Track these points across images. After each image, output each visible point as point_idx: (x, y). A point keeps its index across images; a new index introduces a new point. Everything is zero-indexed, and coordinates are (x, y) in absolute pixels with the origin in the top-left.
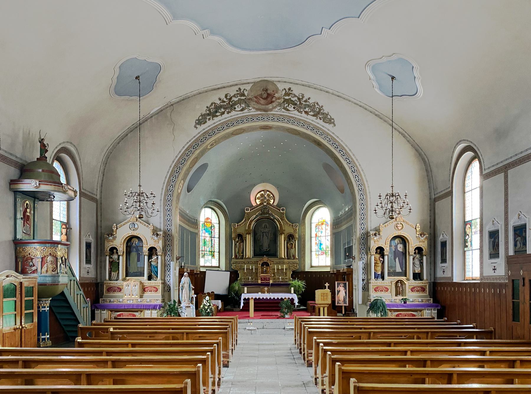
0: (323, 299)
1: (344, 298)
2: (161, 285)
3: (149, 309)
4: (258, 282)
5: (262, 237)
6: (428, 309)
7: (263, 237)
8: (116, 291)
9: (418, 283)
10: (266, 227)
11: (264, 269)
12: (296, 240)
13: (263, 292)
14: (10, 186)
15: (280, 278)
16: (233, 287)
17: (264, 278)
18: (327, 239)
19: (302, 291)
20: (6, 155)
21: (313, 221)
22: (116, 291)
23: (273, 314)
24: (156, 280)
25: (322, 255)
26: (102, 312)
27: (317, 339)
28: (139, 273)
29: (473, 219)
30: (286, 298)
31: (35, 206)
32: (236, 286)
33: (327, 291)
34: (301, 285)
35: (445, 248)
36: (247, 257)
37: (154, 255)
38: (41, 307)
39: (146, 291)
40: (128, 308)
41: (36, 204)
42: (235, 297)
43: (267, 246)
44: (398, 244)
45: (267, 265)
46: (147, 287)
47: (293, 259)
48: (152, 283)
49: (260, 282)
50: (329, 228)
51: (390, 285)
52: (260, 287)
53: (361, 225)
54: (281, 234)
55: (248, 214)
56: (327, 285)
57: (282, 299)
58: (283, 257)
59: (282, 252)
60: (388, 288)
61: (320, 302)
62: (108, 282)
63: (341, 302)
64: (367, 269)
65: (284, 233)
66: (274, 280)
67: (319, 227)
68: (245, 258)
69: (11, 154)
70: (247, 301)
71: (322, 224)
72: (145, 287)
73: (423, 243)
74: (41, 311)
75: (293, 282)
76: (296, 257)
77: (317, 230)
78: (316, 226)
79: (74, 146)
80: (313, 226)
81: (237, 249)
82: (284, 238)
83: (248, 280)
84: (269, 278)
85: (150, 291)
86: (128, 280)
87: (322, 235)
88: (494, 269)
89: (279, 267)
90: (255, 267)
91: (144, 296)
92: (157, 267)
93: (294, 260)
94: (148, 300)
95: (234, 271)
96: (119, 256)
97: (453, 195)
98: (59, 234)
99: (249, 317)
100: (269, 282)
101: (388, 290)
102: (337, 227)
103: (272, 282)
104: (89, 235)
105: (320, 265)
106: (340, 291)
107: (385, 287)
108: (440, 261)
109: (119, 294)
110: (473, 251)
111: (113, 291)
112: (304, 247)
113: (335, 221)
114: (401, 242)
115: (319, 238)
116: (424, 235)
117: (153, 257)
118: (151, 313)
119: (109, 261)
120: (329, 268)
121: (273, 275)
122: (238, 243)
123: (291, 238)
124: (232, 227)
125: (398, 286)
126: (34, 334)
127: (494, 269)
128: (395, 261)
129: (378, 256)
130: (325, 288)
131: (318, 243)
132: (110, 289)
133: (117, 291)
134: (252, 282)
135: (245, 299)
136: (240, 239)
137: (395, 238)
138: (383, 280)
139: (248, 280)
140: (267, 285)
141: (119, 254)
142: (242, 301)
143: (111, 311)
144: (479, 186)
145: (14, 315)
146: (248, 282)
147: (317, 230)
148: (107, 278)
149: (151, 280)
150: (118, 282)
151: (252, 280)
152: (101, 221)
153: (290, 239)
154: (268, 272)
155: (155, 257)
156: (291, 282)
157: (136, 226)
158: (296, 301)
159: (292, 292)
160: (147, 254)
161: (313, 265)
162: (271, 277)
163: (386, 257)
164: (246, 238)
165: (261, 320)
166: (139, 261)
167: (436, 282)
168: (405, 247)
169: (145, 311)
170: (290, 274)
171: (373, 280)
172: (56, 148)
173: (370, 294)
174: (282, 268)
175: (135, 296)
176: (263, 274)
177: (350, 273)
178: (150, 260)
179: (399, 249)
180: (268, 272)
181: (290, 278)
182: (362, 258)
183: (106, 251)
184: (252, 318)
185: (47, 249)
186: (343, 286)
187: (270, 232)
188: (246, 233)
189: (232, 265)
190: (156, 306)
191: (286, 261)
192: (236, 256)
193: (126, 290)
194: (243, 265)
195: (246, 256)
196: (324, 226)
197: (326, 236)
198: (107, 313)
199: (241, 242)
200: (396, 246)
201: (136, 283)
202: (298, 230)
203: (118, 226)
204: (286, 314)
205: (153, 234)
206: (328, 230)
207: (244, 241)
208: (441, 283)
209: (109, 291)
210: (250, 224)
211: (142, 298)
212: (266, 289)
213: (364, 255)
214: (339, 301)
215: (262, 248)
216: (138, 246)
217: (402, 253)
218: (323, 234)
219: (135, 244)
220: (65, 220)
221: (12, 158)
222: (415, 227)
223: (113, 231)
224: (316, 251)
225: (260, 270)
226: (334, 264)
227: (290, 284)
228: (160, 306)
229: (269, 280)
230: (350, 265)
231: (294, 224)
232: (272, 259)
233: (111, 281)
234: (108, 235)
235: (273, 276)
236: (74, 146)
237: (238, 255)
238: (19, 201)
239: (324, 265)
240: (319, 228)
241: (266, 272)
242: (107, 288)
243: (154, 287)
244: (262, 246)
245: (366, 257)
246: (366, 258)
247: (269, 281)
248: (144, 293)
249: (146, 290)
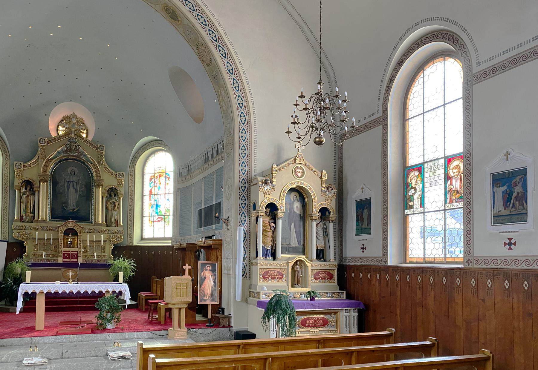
0: (179, 294)
1: (212, 290)
4: (58, 260)
5: (66, 188)
6: (345, 310)
7: (68, 190)
9: (320, 265)
10: (73, 173)
11: (69, 240)
12: (120, 198)
13: (66, 280)
15: (95, 254)
16: (12, 270)
17: (68, 254)
18: (167, 198)
19: (130, 277)
21: (146, 171)
23: (84, 319)
25: (159, 221)
27: (157, 358)
29: (426, 160)
30: (108, 292)
32: (17, 267)
33: (187, 278)
34: (129, 267)
35: (365, 211)
36: (40, 219)
42: (12, 286)
43: (75, 204)
44: (294, 201)
45: (75, 233)
47: (116, 226)
49: (60, 260)
50: (171, 183)
51: (286, 268)
52: (61, 269)
53: (242, 166)
54: (98, 186)
55: (43, 149)
56: (187, 267)
57: (101, 293)
58: (100, 222)
59: (99, 216)
60: (283, 273)
61: (175, 300)
63: (207, 299)
64: (248, 240)
65: (102, 185)
66: (84, 259)
67: (156, 180)
68: (37, 221)
70: (30, 298)
71: (160, 176)
73: (330, 202)
75: (116, 262)
76: (120, 223)
77: (152, 185)
78: (151, 179)
80: (147, 178)
81: (23, 207)
82: (102, 193)
83: (40, 258)
84: (77, 255)
87: (160, 192)
89: (93, 237)
90: (53, 236)
93: (116, 228)
95: (17, 241)
97: (387, 125)
99: (32, 329)
100: (77, 262)
101: (283, 277)
102: (187, 178)
103: (81, 262)
105: (156, 236)
106: (205, 278)
107: (278, 272)
108: (354, 232)
110: (426, 214)
112: (133, 210)
113: (181, 171)
114: (298, 199)
115: (156, 196)
116: (332, 190)
120: (171, 242)
121: (83, 250)
122: (25, 196)
123: (112, 194)
124: (15, 168)
125: (296, 269)
128: (290, 229)
129: (268, 219)
130: (184, 274)
131: (153, 204)
134: (48, 260)
135: (26, 294)
136: (28, 189)
137: (292, 190)
138: (274, 259)
139: (40, 258)
140: (74, 266)
142: (20, 299)
144: (462, 96)
146: (41, 260)
147: (152, 185)
151: (48, 258)
153: (110, 196)
154: (76, 244)
156: (112, 262)
158: (127, 296)
159: (121, 279)
161: (146, 235)
162: (80, 252)
163: (280, 222)
164: (39, 187)
165: (58, 337)
167: (346, 265)
168: (304, 206)
170: (109, 248)
171: (260, 258)
173: (253, 283)
174: (99, 239)
176: (68, 247)
177: (217, 246)
179: (295, 210)
180: (76, 244)
181: (110, 256)
182: (242, 221)
184: (41, 334)
186: (210, 270)
187: (80, 182)
188: (39, 179)
189: (14, 231)
191: (105, 228)
192: (21, 219)
194: (33, 231)
195: (38, 219)
196: (162, 179)
197: (165, 194)
199: (31, 194)
200: (292, 204)
202: (124, 181)
204: (109, 321)
206: (168, 186)
207: (37, 193)
208: (358, 268)
210: (46, 166)
212: (70, 274)
213: (245, 216)
214: (204, 296)
215: (66, 207)
217: (299, 217)
218: (162, 191)
222: (320, 175)
224: (150, 216)
225: (61, 242)
226: (178, 235)
227: (110, 264)
229: (77, 258)
230: (211, 235)
231: (118, 173)
232: (82, 224)
235: (84, 252)
237: (24, 215)
239: (162, 236)
240: (155, 182)
241: (71, 245)
244: (66, 203)
245: (247, 220)
246: (248, 223)
247: (76, 260)
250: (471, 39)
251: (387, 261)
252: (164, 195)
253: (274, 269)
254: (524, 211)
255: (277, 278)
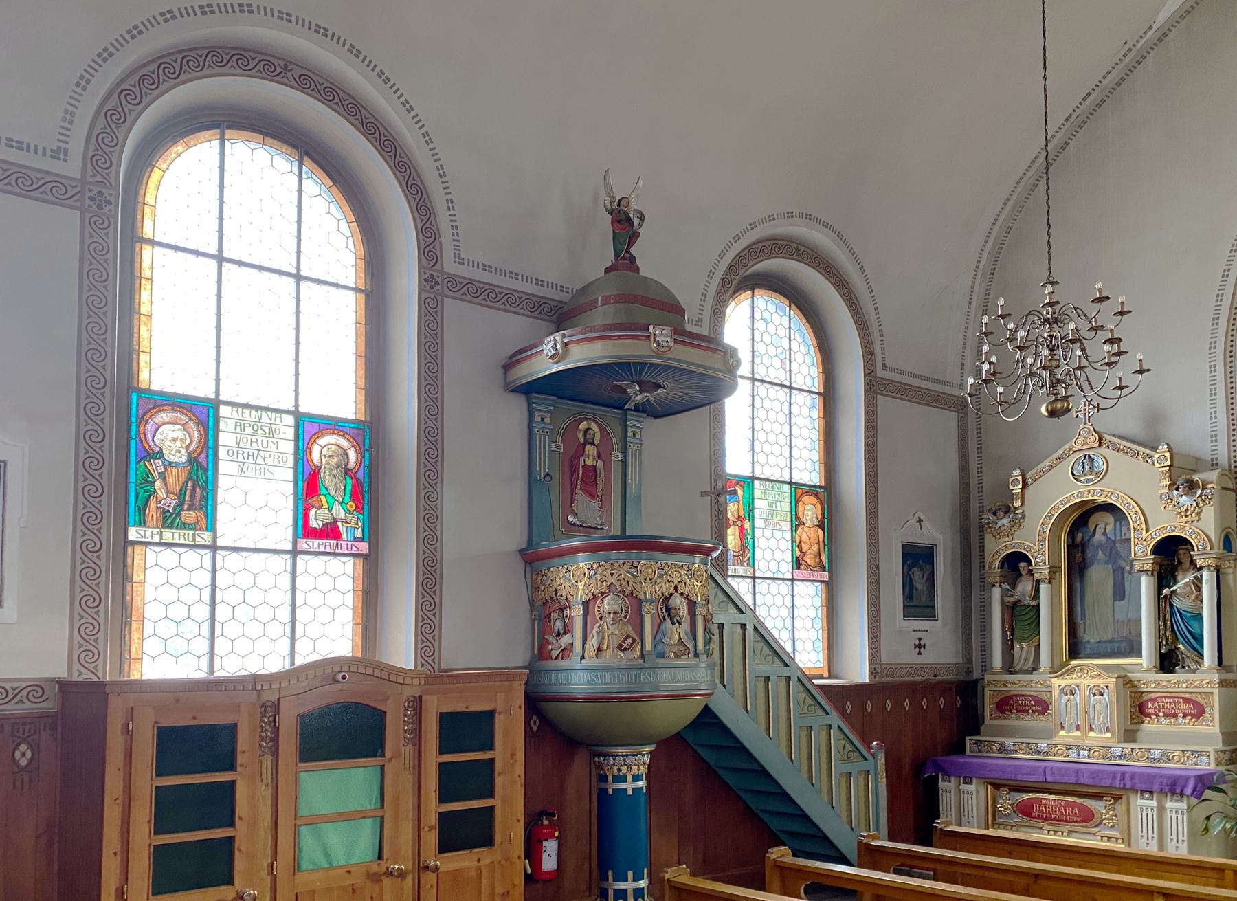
2: (1216, 691)
3: (1151, 793)
8: (1027, 712)
14: (506, 373)
20: (487, 277)
22: (1027, 712)
24: (1194, 671)
26: (964, 787)
28: (1123, 645)
31: (630, 434)
37: (1187, 570)
38: (610, 778)
39: (1149, 715)
40: (1058, 779)
41: (630, 429)
46: (1154, 700)
48: (1178, 681)
62: (997, 680)
69: (514, 275)
72: (1145, 697)
74: (610, 792)
79: (826, 225)
85: (1166, 715)
86: (1072, 670)
88: (920, 646)
91: (1140, 735)
92: (1199, 617)
94: (1156, 753)
96: (1038, 582)
98: (786, 526)
104: (920, 521)
109: (1040, 722)
111: (1018, 711)
117: (1179, 577)
118: (1161, 809)
119: (1003, 603)
126: (499, 889)
127: (920, 646)
132: (1006, 704)
133: (1033, 712)
141: (1037, 576)
143: (997, 786)
145: (378, 820)
148: (997, 662)
149: (1172, 672)
150: (1035, 677)
152: (980, 470)
155: (1184, 580)
157: (1100, 465)
160: (1148, 566)
166: (1122, 597)
169: (1132, 797)
172: (737, 239)
175: (1101, 732)
178: (1166, 591)
183: (990, 568)
185: (600, 570)
190: (1181, 782)
193: (1063, 707)
198: (982, 794)
201: (1101, 682)
203: (1028, 476)
205: (1174, 486)
209: (1003, 712)
211: (1134, 741)
216: (1114, 542)
219: (1105, 533)
220: (811, 474)
221: (11, 159)
223: (1011, 496)
228: (1204, 784)
233: (1011, 673)
234: (995, 514)
236: (826, 225)
238: (547, 420)
242: (997, 700)
243: (1187, 700)
248: (1142, 723)
249: (1150, 708)
250: (1213, 345)
251: (872, 673)
252: (303, 284)
253: (1173, 695)
254: (931, 604)
255: (1033, 712)
